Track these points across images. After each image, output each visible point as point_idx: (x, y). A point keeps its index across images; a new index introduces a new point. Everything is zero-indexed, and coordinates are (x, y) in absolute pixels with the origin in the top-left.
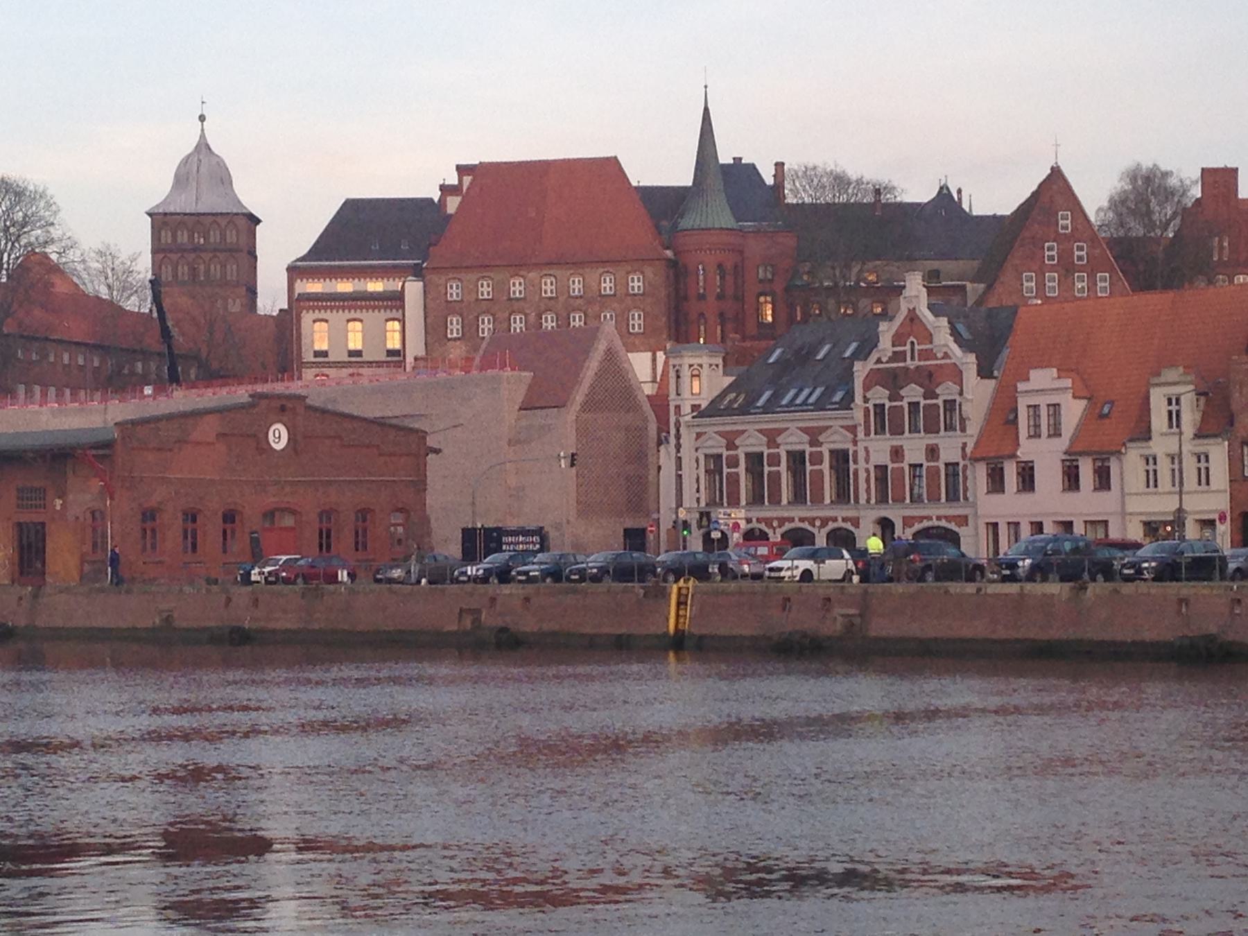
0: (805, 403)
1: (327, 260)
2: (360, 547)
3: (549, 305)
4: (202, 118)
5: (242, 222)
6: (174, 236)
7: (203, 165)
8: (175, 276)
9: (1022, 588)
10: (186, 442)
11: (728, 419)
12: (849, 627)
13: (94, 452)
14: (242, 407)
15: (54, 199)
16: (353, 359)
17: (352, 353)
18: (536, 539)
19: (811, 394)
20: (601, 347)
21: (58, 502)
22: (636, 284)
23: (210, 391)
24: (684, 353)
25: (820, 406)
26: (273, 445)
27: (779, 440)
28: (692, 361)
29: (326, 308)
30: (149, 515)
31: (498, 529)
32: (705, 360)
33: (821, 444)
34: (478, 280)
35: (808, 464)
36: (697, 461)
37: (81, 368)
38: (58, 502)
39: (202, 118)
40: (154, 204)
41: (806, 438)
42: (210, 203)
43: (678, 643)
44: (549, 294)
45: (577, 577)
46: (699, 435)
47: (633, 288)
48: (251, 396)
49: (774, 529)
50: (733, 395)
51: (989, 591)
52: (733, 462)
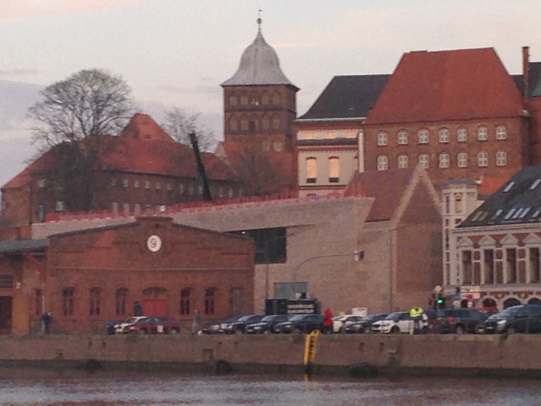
0: (510, 219)
1: (316, 118)
3: (445, 148)
4: (259, 21)
5: (282, 90)
6: (239, 101)
7: (260, 52)
8: (239, 126)
10: (91, 247)
11: (477, 228)
14: (132, 225)
16: (332, 184)
17: (332, 180)
18: (311, 306)
20: (415, 181)
21: (19, 284)
23: (196, 209)
25: (525, 220)
30: (68, 292)
31: (285, 300)
32: (464, 190)
33: (501, 245)
34: (399, 131)
37: (158, 191)
39: (259, 21)
41: (494, 241)
42: (263, 77)
43: (310, 371)
48: (137, 219)
50: (480, 213)
52: (477, 257)
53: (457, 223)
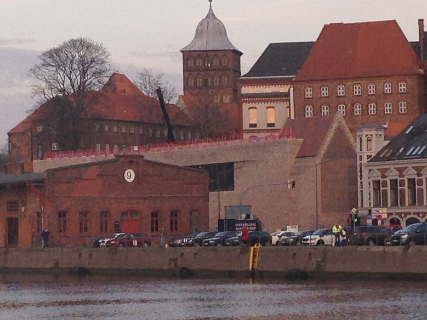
2: (174, 229)
5: (230, 55)
6: (195, 63)
7: (210, 25)
8: (195, 84)
9: (385, 249)
10: (81, 179)
12: (319, 266)
13: (36, 184)
15: (107, 50)
17: (269, 125)
18: (254, 224)
19: (421, 149)
20: (335, 125)
21: (23, 208)
22: (403, 87)
24: (363, 129)
26: (126, 179)
27: (404, 173)
28: (367, 133)
29: (255, 102)
30: (62, 214)
31: (233, 220)
32: (374, 133)
33: (403, 176)
34: (322, 86)
35: (416, 185)
36: (369, 183)
38: (23, 208)
40: (184, 47)
41: (415, 172)
44: (358, 94)
45: (389, 243)
46: (370, 170)
47: (401, 90)
49: (402, 218)
51: (372, 250)
52: (402, 183)
53: (368, 159)
